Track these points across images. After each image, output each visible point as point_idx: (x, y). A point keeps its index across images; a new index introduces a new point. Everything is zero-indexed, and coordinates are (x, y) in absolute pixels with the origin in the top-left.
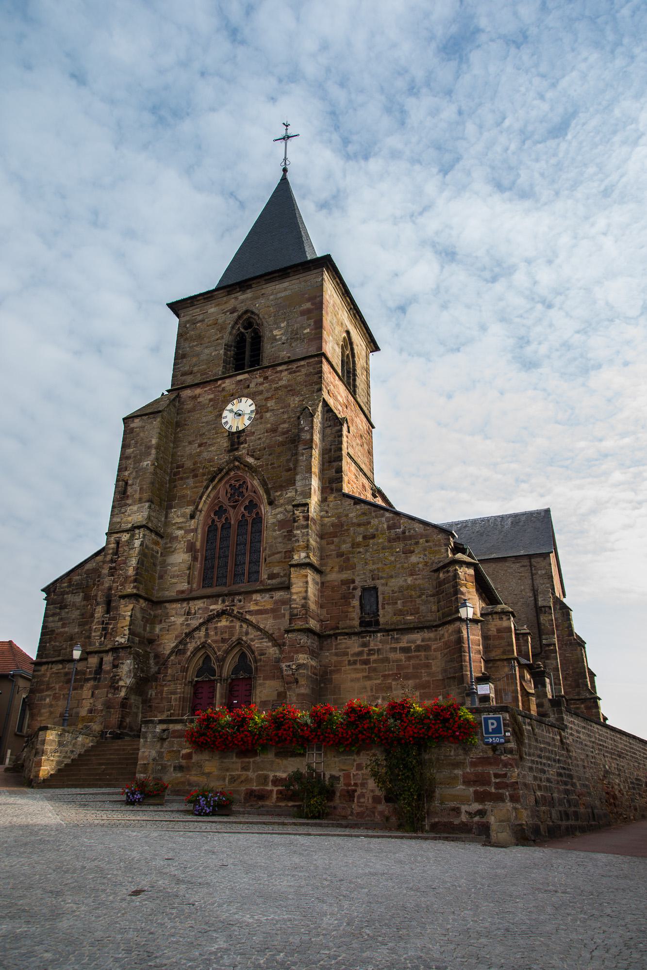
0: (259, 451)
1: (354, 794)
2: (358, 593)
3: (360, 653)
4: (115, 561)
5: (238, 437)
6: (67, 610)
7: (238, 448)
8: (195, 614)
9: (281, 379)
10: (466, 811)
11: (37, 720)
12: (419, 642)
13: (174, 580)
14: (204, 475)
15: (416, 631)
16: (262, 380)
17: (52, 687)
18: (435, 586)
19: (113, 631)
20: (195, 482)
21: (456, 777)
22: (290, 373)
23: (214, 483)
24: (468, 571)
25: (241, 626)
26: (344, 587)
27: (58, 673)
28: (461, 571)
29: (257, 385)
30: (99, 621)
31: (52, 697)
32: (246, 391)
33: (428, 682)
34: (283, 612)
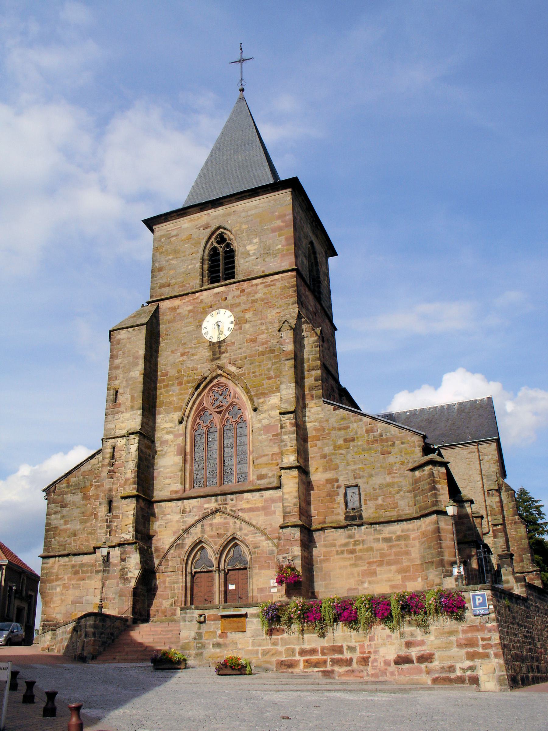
0: (241, 360)
1: (368, 660)
2: (342, 491)
3: (346, 544)
4: (113, 465)
5: (219, 347)
6: (67, 509)
7: (220, 357)
8: (190, 512)
11: (50, 607)
12: (399, 533)
13: (167, 481)
14: (188, 382)
15: (396, 523)
16: (238, 293)
17: (61, 578)
19: (117, 529)
20: (180, 390)
22: (266, 287)
23: (199, 390)
25: (235, 523)
27: (65, 565)
28: (435, 469)
29: (234, 297)
33: (409, 566)
34: (273, 509)
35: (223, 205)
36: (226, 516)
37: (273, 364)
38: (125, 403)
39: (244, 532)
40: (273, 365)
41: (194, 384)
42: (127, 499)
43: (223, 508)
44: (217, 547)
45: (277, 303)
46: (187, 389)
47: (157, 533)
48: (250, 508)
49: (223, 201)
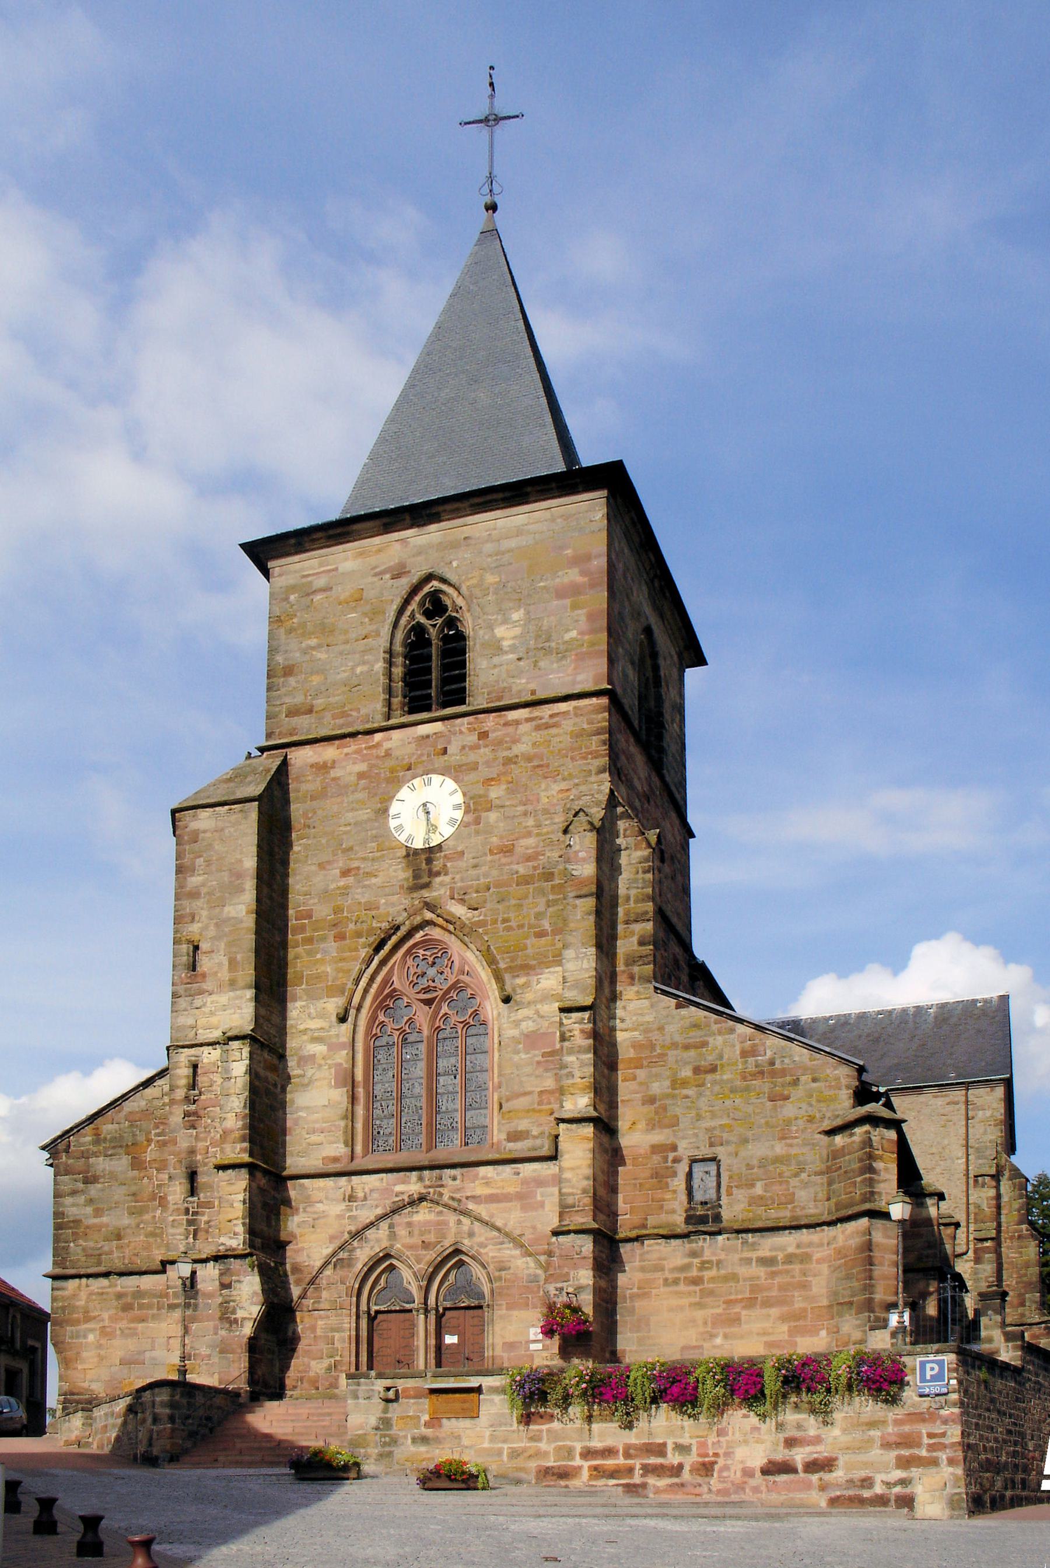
0: (477, 892)
2: (683, 1168)
4: (195, 1101)
5: (429, 861)
6: (99, 1186)
8: (365, 1198)
9: (515, 741)
10: (882, 1481)
11: (76, 1369)
12: (791, 1250)
13: (314, 1138)
14: (358, 934)
16: (473, 738)
17: (95, 1318)
18: (825, 1157)
20: (340, 950)
21: (870, 1441)
22: (538, 728)
23: (383, 953)
24: (886, 1134)
25: (459, 1222)
26: (656, 1158)
27: (102, 1294)
28: (876, 1133)
29: (463, 748)
30: (178, 1209)
31: (98, 1332)
32: (440, 761)
34: (539, 1198)
35: (440, 521)
36: (441, 1208)
37: (549, 904)
38: (216, 973)
39: (478, 1239)
40: (549, 906)
41: (371, 939)
42: (230, 1171)
43: (434, 1194)
44: (421, 1266)
45: (561, 769)
46: (356, 950)
47: (295, 1237)
48: (492, 1194)
49: (440, 508)
